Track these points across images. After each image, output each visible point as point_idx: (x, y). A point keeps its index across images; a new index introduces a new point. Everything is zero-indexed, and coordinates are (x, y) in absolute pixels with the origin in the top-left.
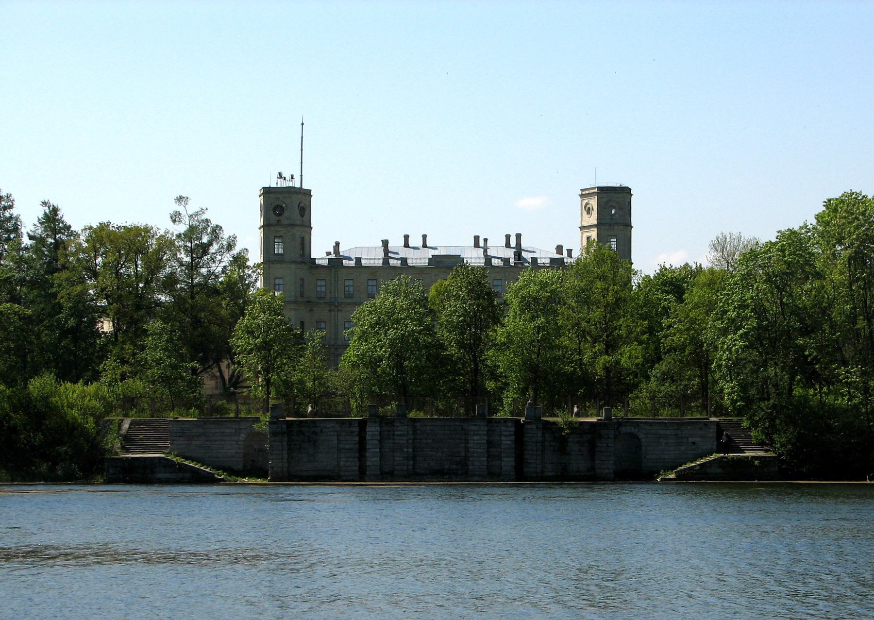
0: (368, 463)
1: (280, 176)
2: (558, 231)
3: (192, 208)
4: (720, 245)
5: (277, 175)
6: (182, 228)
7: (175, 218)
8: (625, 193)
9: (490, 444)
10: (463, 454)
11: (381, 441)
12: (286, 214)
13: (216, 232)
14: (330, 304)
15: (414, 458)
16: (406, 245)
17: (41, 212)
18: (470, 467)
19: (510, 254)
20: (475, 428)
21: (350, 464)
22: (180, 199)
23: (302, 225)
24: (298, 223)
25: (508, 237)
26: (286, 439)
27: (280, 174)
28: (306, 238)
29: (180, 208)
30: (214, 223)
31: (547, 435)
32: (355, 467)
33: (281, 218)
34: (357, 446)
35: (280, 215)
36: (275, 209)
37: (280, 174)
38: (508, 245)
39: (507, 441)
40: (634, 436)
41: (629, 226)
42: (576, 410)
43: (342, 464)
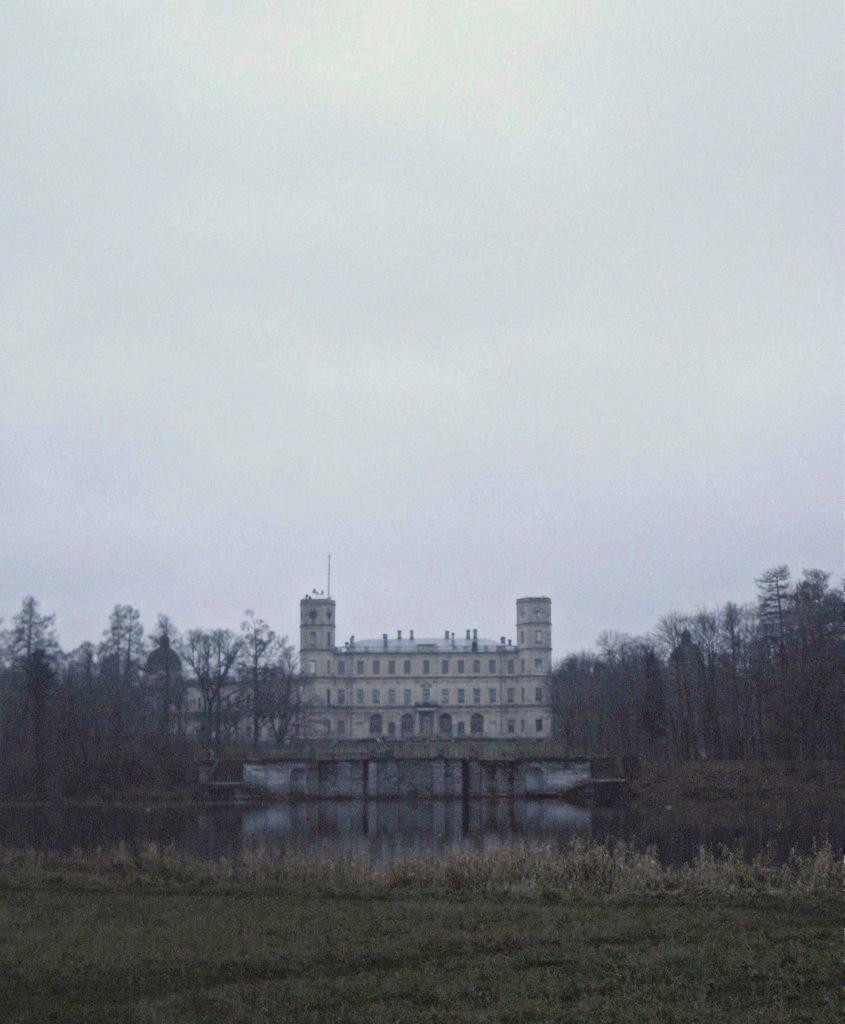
1: (314, 591)
2: (500, 627)
4: (604, 640)
7: (244, 625)
8: (547, 601)
9: (447, 775)
12: (319, 617)
16: (399, 638)
17: (158, 633)
22: (249, 612)
25: (468, 631)
30: (271, 629)
38: (468, 637)
42: (592, 670)
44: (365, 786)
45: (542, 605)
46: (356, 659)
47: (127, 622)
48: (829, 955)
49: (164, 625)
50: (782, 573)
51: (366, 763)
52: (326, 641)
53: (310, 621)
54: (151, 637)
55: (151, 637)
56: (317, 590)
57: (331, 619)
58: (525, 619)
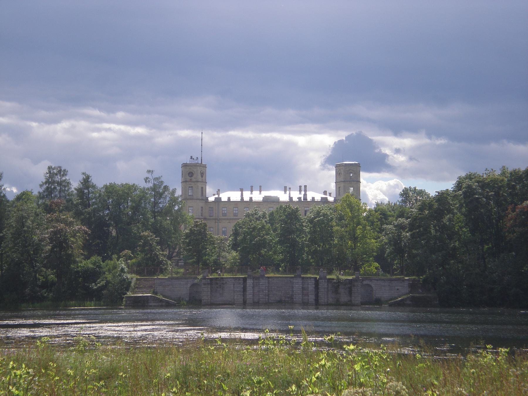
0: (248, 297)
1: (191, 158)
3: (155, 175)
5: (190, 157)
6: (150, 185)
10: (291, 293)
11: (253, 287)
12: (194, 176)
13: (166, 188)
14: (215, 219)
15: (268, 295)
17: (81, 177)
18: (295, 300)
20: (297, 281)
21: (239, 298)
22: (149, 171)
23: (202, 182)
24: (200, 180)
26: (209, 286)
27: (191, 157)
28: (204, 188)
29: (149, 175)
31: (329, 285)
32: (241, 300)
33: (192, 178)
34: (242, 290)
35: (191, 176)
36: (189, 174)
37: (191, 157)
39: (311, 287)
40: (369, 286)
41: (359, 182)
43: (236, 298)
44: (244, 295)
47: (58, 178)
48: (207, 353)
49: (86, 181)
51: (245, 280)
52: (200, 193)
53: (188, 178)
54: (75, 189)
55: (75, 189)
56: (193, 157)
57: (204, 178)
58: (200, 185)
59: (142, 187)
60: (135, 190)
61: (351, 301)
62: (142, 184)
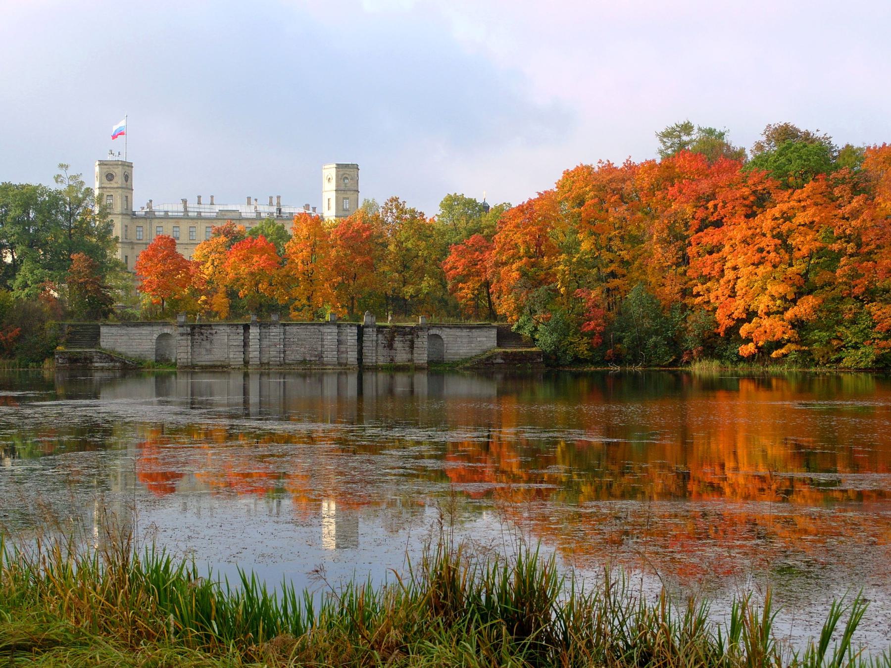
3: (71, 172)
7: (57, 178)
8: (355, 167)
12: (116, 179)
15: (285, 352)
16: (199, 203)
19: (274, 209)
20: (329, 330)
22: (61, 166)
23: (127, 188)
25: (271, 198)
34: (242, 344)
36: (107, 176)
38: (271, 204)
40: (438, 337)
45: (348, 171)
46: (155, 223)
50: (687, 128)
51: (246, 328)
57: (129, 183)
59: (53, 189)
60: (42, 195)
61: (411, 360)
62: (53, 186)
